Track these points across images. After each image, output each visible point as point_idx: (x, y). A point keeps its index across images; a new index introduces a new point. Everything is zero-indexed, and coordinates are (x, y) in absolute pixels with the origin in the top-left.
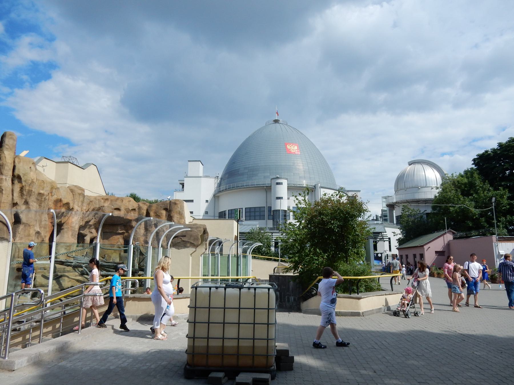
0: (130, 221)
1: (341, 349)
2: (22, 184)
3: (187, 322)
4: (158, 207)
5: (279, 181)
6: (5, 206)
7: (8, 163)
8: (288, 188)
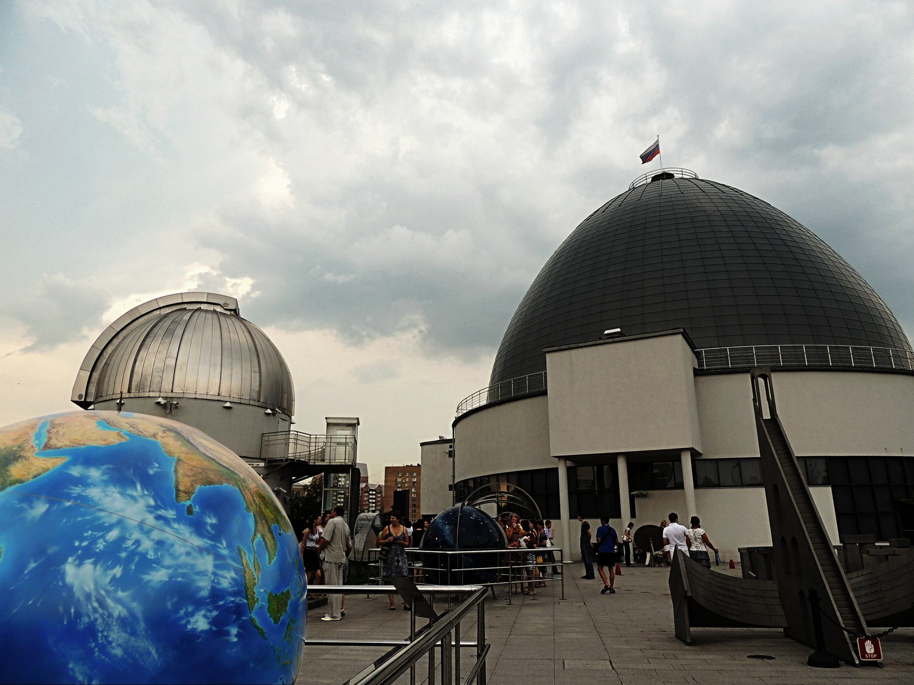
1: (643, 149)
3: (386, 467)
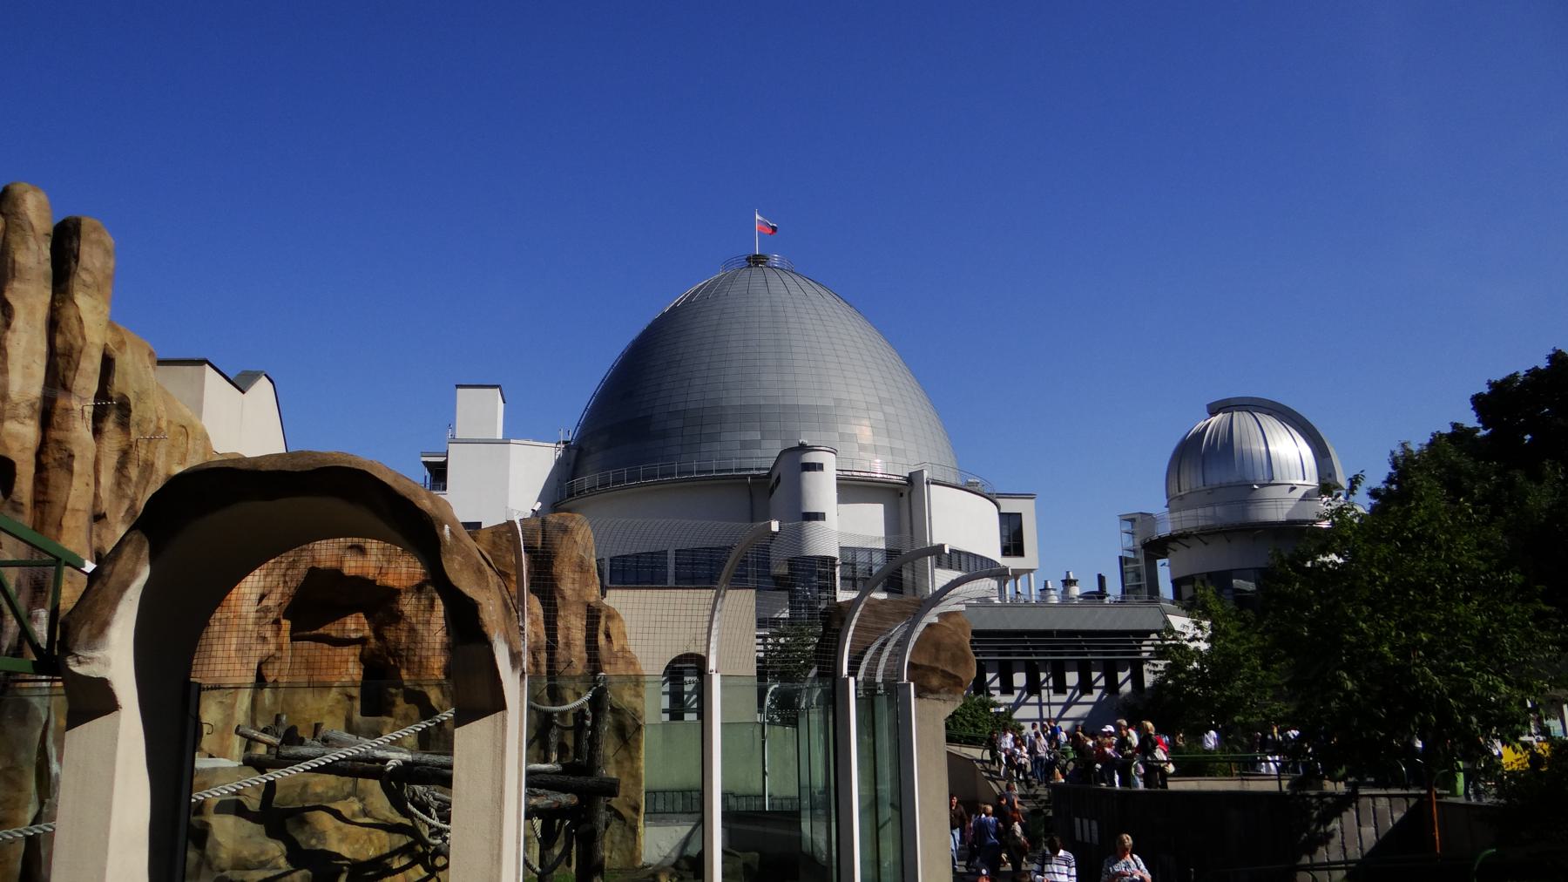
0: (393, 594)
2: (129, 434)
3: (1020, 515)
4: (497, 540)
5: (811, 457)
6: (77, 527)
7: (91, 343)
8: (838, 485)
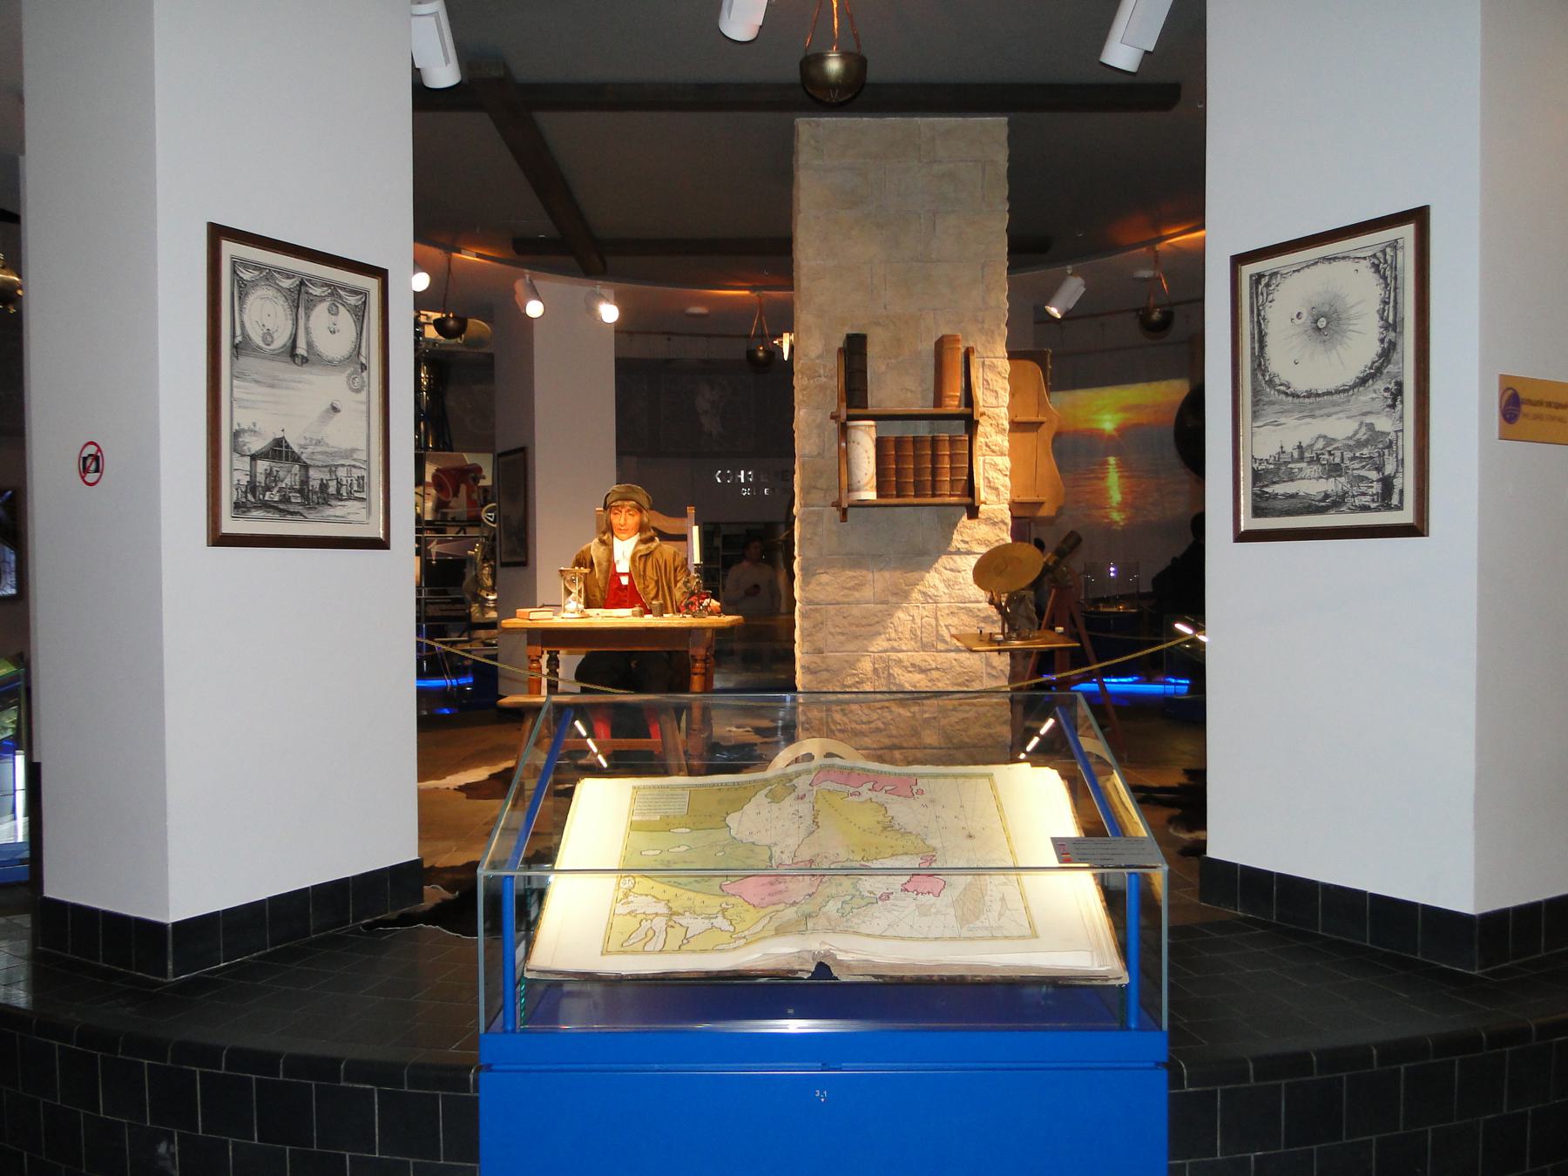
3: (1232, 257)
